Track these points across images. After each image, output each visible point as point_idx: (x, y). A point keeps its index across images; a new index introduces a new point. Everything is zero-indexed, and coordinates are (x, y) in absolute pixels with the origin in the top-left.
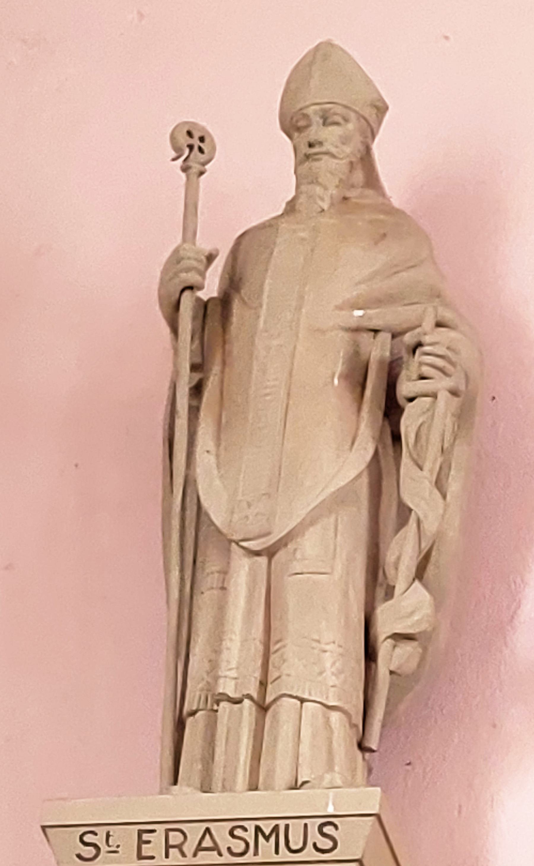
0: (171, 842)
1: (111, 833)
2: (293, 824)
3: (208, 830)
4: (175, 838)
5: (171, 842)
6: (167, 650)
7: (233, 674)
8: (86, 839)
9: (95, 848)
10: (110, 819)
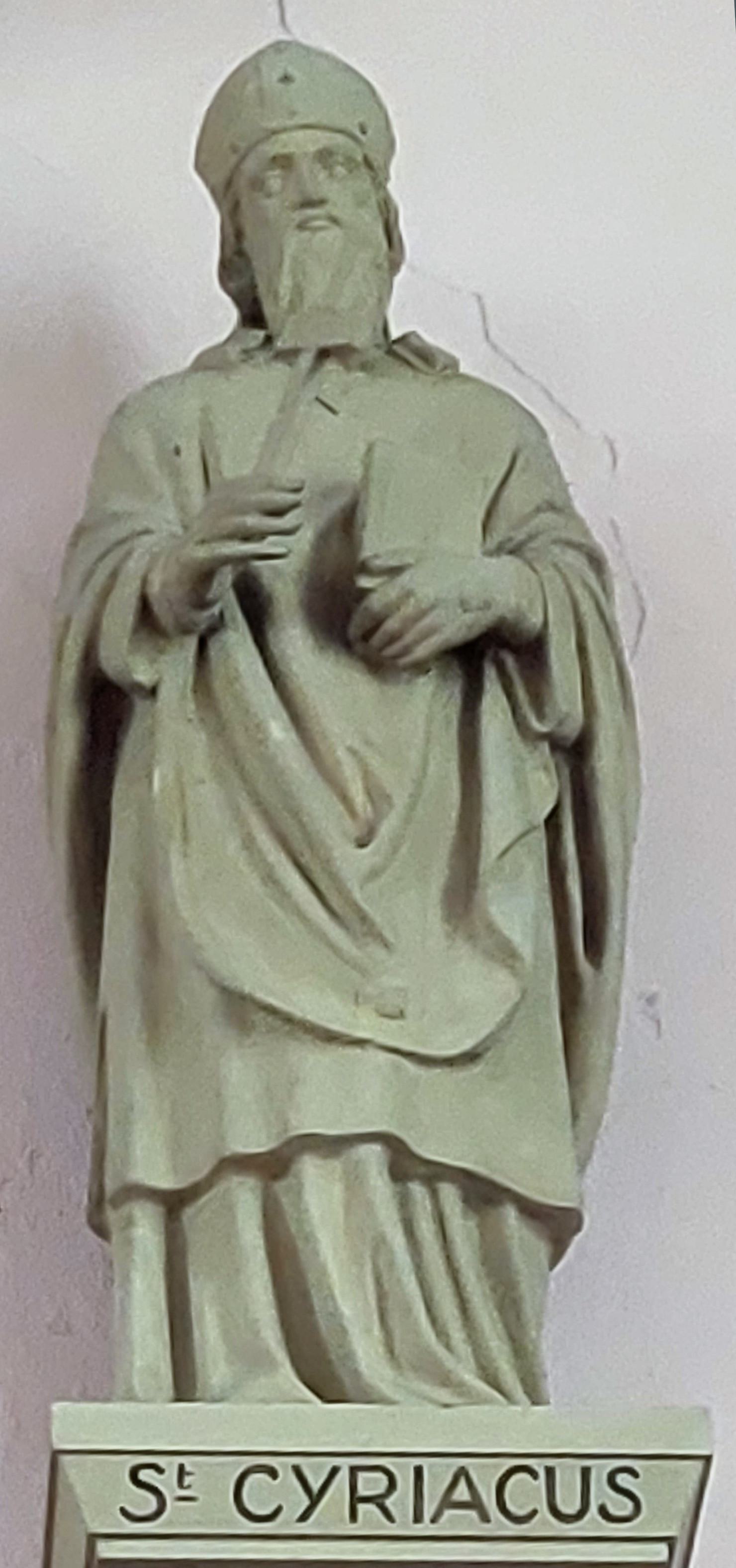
0: (362, 1491)
1: (188, 1468)
2: (431, 1466)
3: (462, 1472)
4: (371, 1484)
5: (362, 1491)
6: (617, 1002)
7: (280, 806)
8: (143, 1475)
9: (158, 1502)
10: (385, 1445)
